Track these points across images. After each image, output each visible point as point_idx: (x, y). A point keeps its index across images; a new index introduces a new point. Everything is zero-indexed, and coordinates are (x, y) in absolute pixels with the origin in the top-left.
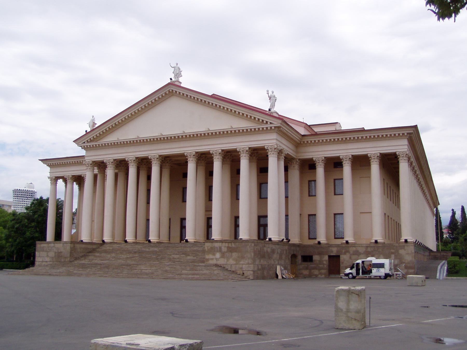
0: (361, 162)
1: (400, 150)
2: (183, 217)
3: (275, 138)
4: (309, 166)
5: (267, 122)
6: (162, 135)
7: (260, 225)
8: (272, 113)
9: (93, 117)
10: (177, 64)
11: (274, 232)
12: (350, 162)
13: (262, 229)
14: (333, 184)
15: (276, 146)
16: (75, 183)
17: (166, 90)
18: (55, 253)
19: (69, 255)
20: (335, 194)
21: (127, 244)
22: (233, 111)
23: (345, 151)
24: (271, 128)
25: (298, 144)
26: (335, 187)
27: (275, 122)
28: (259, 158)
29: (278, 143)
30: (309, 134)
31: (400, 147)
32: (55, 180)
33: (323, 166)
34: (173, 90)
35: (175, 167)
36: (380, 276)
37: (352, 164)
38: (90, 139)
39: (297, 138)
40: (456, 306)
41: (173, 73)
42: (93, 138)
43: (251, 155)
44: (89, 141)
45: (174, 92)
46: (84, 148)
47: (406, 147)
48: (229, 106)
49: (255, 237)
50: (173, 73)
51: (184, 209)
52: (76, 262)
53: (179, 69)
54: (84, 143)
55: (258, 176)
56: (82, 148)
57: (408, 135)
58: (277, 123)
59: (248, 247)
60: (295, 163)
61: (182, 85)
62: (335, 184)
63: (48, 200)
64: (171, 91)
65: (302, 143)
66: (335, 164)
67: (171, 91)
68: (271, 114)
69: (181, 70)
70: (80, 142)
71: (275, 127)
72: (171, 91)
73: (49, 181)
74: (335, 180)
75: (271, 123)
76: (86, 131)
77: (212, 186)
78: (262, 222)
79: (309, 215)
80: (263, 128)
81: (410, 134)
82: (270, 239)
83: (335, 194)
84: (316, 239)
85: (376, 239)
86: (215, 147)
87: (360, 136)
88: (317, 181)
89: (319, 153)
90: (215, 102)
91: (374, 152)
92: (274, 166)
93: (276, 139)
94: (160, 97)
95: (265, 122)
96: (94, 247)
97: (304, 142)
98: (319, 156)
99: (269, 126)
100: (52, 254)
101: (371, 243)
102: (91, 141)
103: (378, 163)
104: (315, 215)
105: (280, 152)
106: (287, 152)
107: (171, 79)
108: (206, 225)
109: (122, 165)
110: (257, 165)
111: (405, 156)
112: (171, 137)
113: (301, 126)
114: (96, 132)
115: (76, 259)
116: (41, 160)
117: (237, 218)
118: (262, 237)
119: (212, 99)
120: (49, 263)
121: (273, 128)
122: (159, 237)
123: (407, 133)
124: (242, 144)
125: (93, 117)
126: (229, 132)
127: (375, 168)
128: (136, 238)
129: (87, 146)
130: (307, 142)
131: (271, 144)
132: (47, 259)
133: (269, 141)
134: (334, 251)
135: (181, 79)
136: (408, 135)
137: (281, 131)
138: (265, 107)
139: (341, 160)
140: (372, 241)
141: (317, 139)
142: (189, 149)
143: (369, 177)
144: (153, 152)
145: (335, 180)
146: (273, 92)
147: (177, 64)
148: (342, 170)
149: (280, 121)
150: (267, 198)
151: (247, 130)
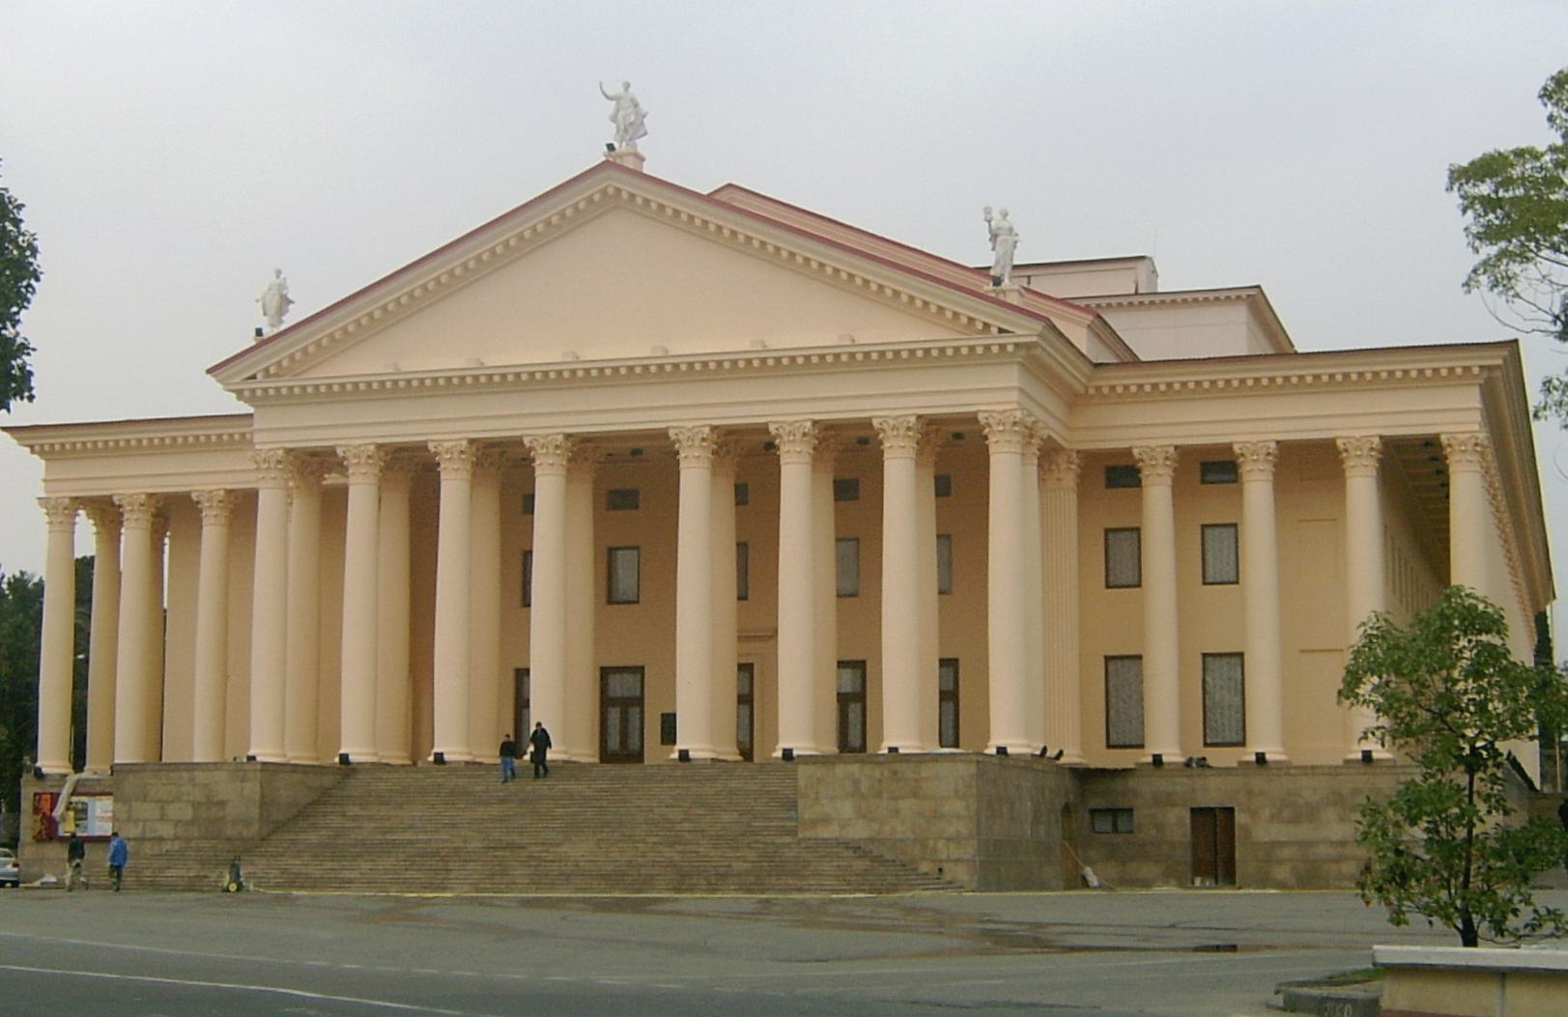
0: (1309, 466)
1: (1453, 428)
2: (520, 666)
3: (1015, 384)
4: (1120, 473)
5: (986, 326)
6: (482, 366)
7: (606, 701)
8: (621, 156)
9: (279, 273)
10: (627, 86)
11: (1009, 726)
12: (1269, 468)
13: (614, 714)
14: (1102, 541)
15: (1019, 414)
16: (82, 512)
17: (592, 189)
18: (196, 805)
19: (255, 812)
20: (1107, 531)
21: (1207, 772)
22: (698, 222)
23: (1252, 427)
24: (1003, 347)
25: (1077, 395)
26: (1216, 558)
27: (1022, 327)
28: (956, 456)
29: (1031, 406)
30: (1113, 360)
31: (1454, 416)
32: (63, 511)
33: (1169, 482)
34: (618, 191)
35: (628, 483)
36: (843, 700)
37: (1275, 475)
38: (279, 364)
39: (1075, 375)
40: (1217, 948)
41: (614, 119)
42: (278, 360)
43: (476, 465)
44: (272, 370)
45: (625, 195)
46: (240, 394)
47: (1477, 416)
48: (947, 300)
49: (831, 748)
50: (614, 119)
51: (17, 819)
52: (1538, 932)
53: (636, 105)
54: (254, 377)
55: (598, 523)
56: (33, 451)
57: (1023, 352)
58: (1026, 331)
59: (1375, 680)
60: (1063, 466)
61: (1167, 282)
62: (1106, 540)
63: (40, 586)
64: (611, 191)
65: (1092, 391)
66: (1213, 468)
67: (614, 190)
68: (1001, 297)
69: (644, 107)
70: (235, 375)
71: (1017, 345)
72: (611, 191)
73: (41, 515)
74: (1204, 527)
75: (1001, 331)
76: (259, 332)
77: (533, 496)
78: (619, 686)
79: (1108, 659)
80: (972, 348)
81: (1490, 368)
82: (439, 759)
83: (1107, 531)
84: (1142, 746)
85: (1002, 743)
86: (790, 411)
87: (1162, 381)
88: (735, 597)
89: (1154, 431)
90: (729, 222)
91: (1358, 434)
92: (1008, 475)
93: (1021, 390)
94: (569, 212)
95: (980, 326)
96: (328, 781)
97: (1098, 389)
98: (1153, 443)
99: (994, 340)
100: (182, 811)
101: (1347, 762)
102: (411, 842)
103: (1374, 473)
104: (1140, 657)
105: (1030, 433)
106: (1045, 433)
107: (611, 147)
108: (598, 694)
109: (413, 474)
110: (597, 483)
111: (798, 437)
112: (616, 370)
113: (1079, 324)
114: (291, 345)
115: (279, 827)
116: (209, 371)
117: (522, 675)
118: (854, 709)
119: (706, 206)
120: (167, 846)
121: (1010, 348)
122: (223, 750)
123: (1482, 367)
124: (895, 405)
125: (279, 273)
126: (785, 361)
127: (1362, 490)
128: (223, 750)
129: (266, 390)
130: (1113, 388)
131: (1000, 408)
132: (165, 830)
133: (994, 396)
134: (1212, 793)
135: (642, 146)
136: (1485, 375)
137: (1034, 359)
138: (980, 255)
139: (673, 443)
140: (1352, 756)
141: (1132, 379)
142: (688, 416)
143: (1337, 521)
144: (542, 423)
145: (1204, 527)
146: (1005, 215)
147: (627, 86)
148: (1240, 493)
149: (1038, 326)
150: (837, 540)
151: (927, 351)
